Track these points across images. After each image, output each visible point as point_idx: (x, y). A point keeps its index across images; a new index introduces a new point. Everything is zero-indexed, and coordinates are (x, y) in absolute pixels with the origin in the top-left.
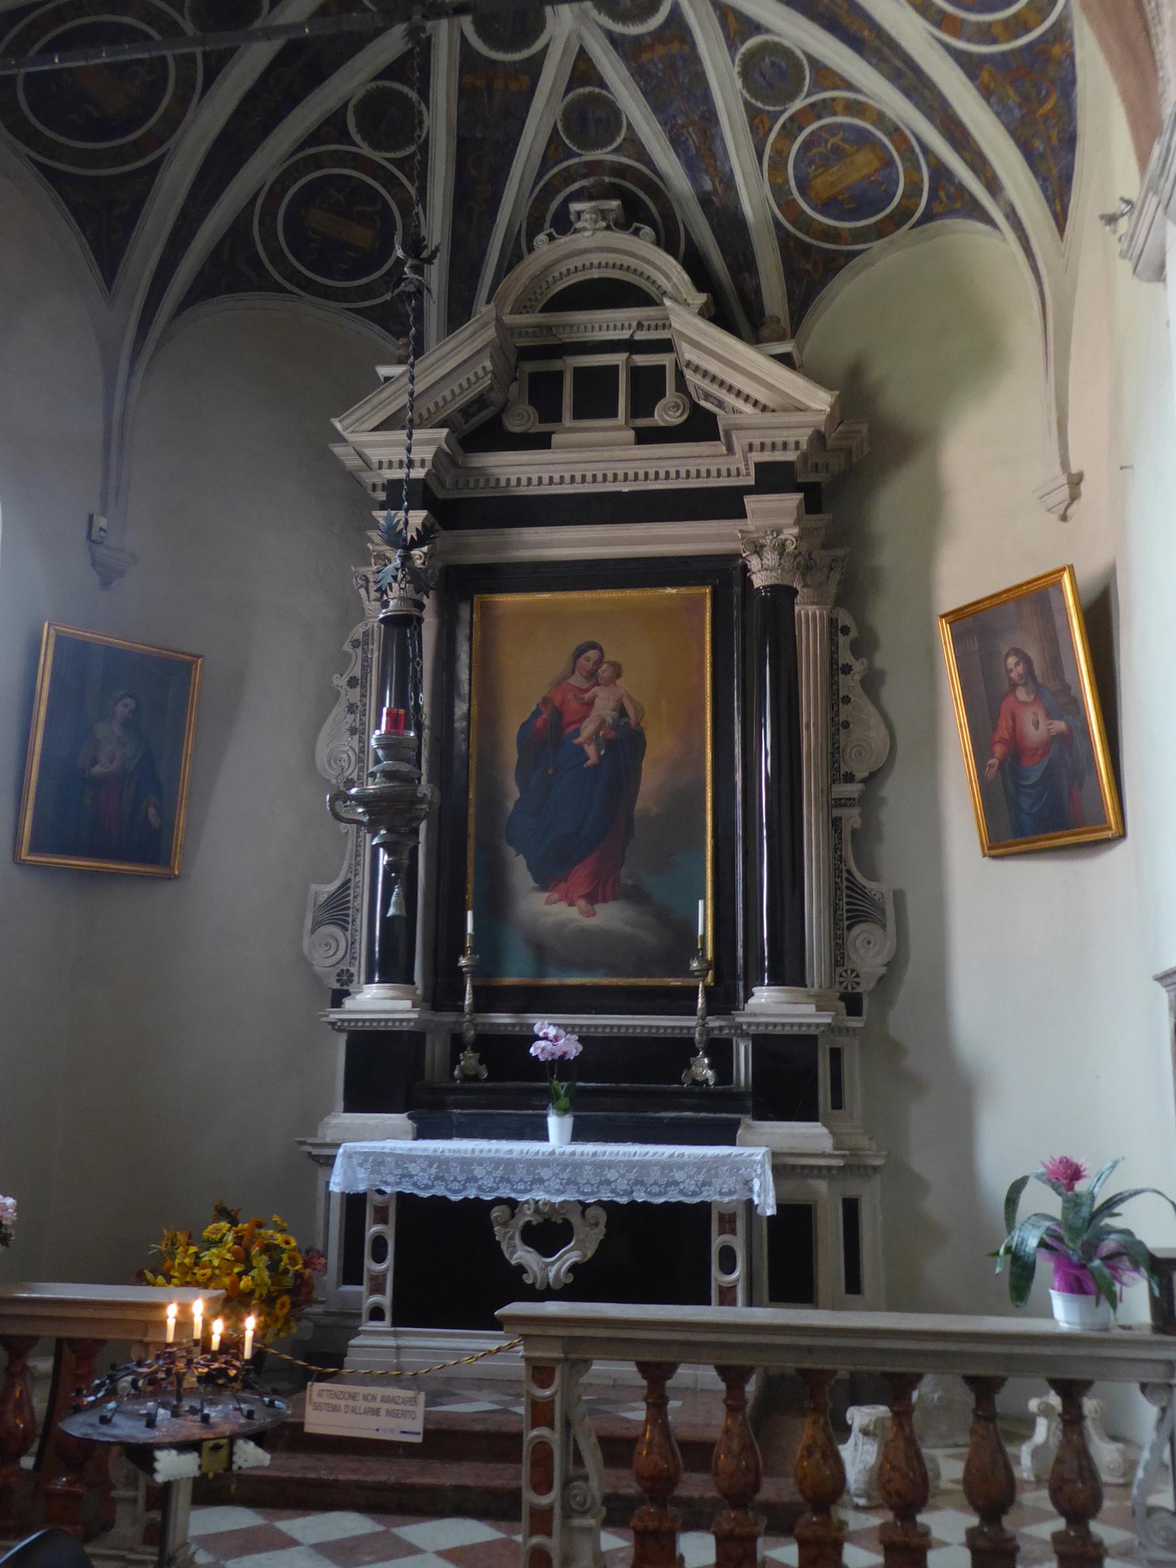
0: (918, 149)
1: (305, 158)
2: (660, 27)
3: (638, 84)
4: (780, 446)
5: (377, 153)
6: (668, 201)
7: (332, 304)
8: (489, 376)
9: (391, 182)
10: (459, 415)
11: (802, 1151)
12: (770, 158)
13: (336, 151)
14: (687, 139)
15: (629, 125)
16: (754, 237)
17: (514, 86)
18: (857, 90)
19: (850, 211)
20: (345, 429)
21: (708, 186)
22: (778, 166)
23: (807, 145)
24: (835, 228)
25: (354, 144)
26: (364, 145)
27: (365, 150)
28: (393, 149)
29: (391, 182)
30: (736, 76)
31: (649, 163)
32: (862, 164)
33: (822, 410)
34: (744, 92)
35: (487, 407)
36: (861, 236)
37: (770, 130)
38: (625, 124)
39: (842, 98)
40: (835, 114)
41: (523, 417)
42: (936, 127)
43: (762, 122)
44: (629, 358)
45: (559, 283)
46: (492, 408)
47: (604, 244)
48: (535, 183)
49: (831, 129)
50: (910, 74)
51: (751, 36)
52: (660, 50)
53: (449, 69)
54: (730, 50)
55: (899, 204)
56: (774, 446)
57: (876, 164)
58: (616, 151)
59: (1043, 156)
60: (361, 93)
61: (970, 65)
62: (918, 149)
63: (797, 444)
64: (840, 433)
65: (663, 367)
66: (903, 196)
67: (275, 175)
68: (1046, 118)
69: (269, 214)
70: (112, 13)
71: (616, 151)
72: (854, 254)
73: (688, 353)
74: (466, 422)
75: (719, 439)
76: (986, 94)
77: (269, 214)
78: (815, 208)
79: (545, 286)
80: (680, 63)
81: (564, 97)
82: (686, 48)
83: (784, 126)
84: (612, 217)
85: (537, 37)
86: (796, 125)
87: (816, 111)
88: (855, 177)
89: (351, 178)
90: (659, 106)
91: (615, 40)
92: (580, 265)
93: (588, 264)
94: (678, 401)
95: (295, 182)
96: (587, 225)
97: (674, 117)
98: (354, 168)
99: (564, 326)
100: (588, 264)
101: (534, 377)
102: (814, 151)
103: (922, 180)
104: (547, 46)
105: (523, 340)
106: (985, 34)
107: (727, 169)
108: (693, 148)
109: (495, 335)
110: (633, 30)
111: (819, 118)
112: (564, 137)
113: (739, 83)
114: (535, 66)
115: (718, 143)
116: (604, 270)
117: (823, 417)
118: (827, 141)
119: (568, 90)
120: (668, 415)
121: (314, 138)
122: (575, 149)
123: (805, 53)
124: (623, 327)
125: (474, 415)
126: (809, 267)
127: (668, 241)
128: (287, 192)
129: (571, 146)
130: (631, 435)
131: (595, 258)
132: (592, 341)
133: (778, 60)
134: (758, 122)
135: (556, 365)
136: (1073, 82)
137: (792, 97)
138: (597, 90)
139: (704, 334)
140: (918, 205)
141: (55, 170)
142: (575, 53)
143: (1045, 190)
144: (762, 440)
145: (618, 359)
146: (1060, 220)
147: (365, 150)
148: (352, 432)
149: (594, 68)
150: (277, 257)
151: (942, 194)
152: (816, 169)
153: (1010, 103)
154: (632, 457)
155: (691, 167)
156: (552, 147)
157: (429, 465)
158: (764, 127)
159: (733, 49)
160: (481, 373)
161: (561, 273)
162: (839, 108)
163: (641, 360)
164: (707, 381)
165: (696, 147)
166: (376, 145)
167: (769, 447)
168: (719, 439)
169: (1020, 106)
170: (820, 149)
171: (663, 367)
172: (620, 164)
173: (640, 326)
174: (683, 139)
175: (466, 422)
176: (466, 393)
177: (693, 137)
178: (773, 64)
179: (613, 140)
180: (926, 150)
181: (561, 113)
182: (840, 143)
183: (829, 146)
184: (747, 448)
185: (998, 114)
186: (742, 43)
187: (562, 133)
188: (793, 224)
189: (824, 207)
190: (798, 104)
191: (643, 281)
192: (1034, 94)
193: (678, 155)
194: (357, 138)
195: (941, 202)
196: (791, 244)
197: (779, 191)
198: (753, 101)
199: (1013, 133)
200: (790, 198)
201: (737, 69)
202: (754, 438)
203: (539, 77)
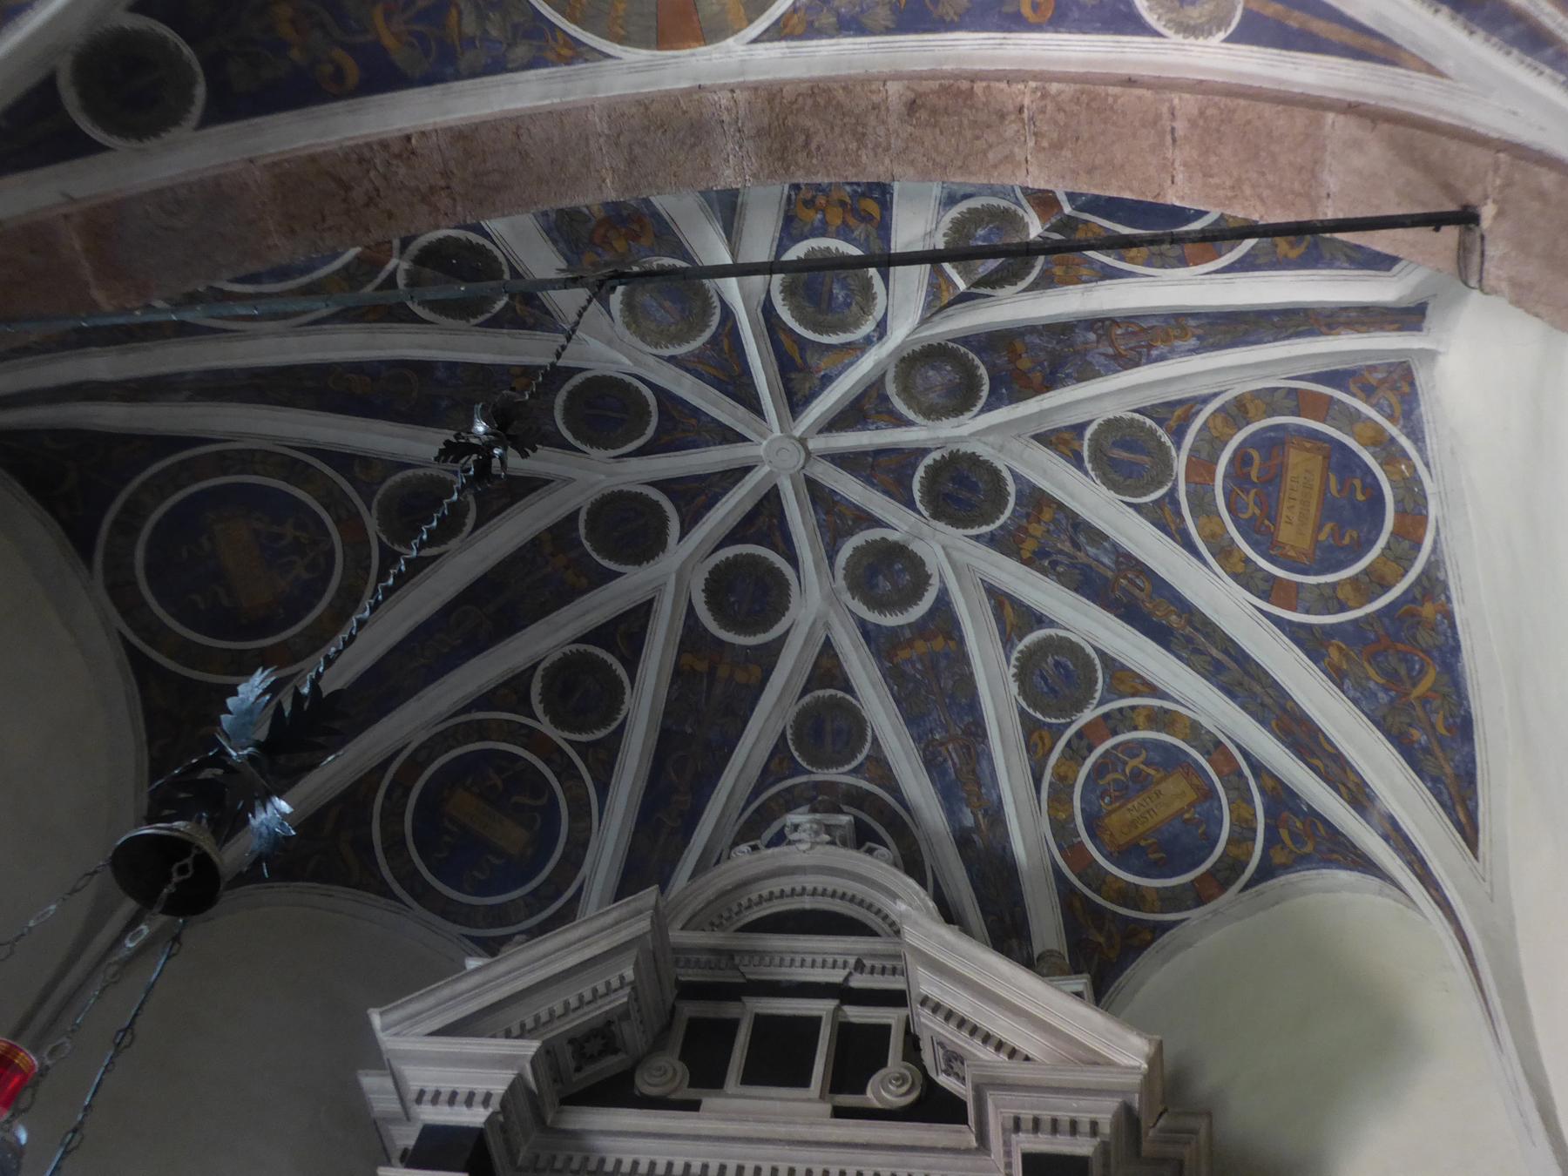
0: (1247, 771)
1: (468, 723)
2: (922, 617)
3: (891, 690)
4: (1065, 1126)
5: (559, 732)
6: (915, 841)
7: (449, 926)
8: (627, 990)
9: (566, 771)
10: (568, 1050)
11: (723, 1134)
12: (1051, 784)
13: (508, 722)
14: (945, 760)
15: (875, 740)
16: (1027, 888)
17: (740, 677)
18: (1164, 696)
19: (1156, 863)
20: (385, 1028)
21: (969, 821)
22: (1060, 795)
23: (1099, 770)
24: (1137, 886)
25: (534, 717)
26: (546, 720)
27: (546, 726)
28: (579, 729)
29: (566, 771)
30: (1011, 679)
31: (895, 789)
32: (1173, 795)
33: (1133, 1068)
34: (1020, 700)
35: (615, 1051)
36: (1173, 900)
37: (1051, 749)
38: (869, 738)
39: (1144, 707)
40: (1135, 728)
41: (665, 1073)
42: (1271, 731)
43: (1041, 738)
44: (838, 1008)
45: (755, 909)
46: (621, 1056)
47: (827, 862)
48: (748, 803)
49: (1131, 748)
50: (1232, 665)
51: (1031, 630)
52: (921, 646)
53: (667, 639)
54: (1004, 647)
55: (1225, 853)
56: (1055, 1126)
57: (1192, 796)
58: (854, 771)
59: (1427, 750)
60: (557, 655)
61: (1310, 642)
62: (1247, 771)
63: (1094, 1125)
64: (1162, 1130)
65: (887, 1028)
66: (1229, 842)
67: (423, 737)
68: (1424, 700)
69: (402, 784)
70: (286, 480)
71: (854, 771)
72: (1166, 927)
73: (926, 984)
74: (578, 1069)
75: (965, 1121)
76: (1337, 677)
77: (402, 784)
78: (1108, 857)
79: (735, 909)
80: (943, 663)
81: (799, 698)
82: (952, 644)
83: (1069, 744)
84: (838, 833)
85: (777, 620)
86: (1084, 743)
87: (1111, 723)
88: (1163, 814)
89: (518, 758)
90: (913, 717)
91: (868, 633)
92: (788, 889)
93: (798, 889)
94: (907, 1073)
95: (446, 752)
96: (804, 836)
97: (931, 730)
98: (525, 747)
99: (752, 953)
100: (798, 889)
101: (694, 1024)
102: (1110, 777)
103: (1255, 815)
104: (787, 632)
105: (690, 971)
106: (1330, 600)
107: (995, 796)
108: (952, 771)
109: (649, 928)
110: (890, 620)
111: (1115, 733)
112: (792, 748)
113: (1014, 688)
114: (768, 656)
115: (984, 764)
116: (820, 970)
117: (1136, 1079)
118: (1125, 763)
119: (805, 691)
120: (888, 1091)
121: (485, 700)
122: (804, 764)
123: (1096, 649)
124: (834, 965)
125: (592, 1059)
126: (1101, 940)
127: (913, 864)
128: (433, 760)
129: (799, 760)
130: (828, 1108)
131: (810, 881)
132: (790, 981)
133: (1063, 660)
134: (1036, 738)
135: (730, 1010)
136: (1456, 649)
137: (1079, 706)
138: (840, 694)
139: (953, 950)
140: (1250, 854)
141: (146, 657)
142: (820, 644)
143: (1437, 795)
144: (1036, 1112)
145: (822, 1008)
146: (1469, 832)
147: (546, 726)
148: (396, 1034)
149: (840, 666)
150: (394, 845)
151: (1284, 834)
152: (1111, 803)
153: (1372, 685)
154: (824, 1138)
155: (949, 796)
156: (776, 760)
157: (495, 1105)
158: (1044, 744)
159: (1009, 646)
160: (615, 983)
161: (760, 896)
162: (1141, 720)
163: (857, 1014)
164: (952, 1026)
165: (955, 772)
166: (558, 722)
167: (1046, 1126)
168: (965, 1121)
169: (1386, 690)
170: (1117, 776)
171: (887, 1028)
172: (858, 789)
173: (859, 966)
174: (940, 759)
175: (578, 1069)
176: (586, 1009)
177: (952, 757)
178: (1057, 664)
179: (854, 757)
180: (1258, 768)
181: (792, 718)
182: (1142, 766)
183: (1127, 771)
184: (1010, 1124)
185: (1355, 701)
186: (1020, 640)
187: (790, 743)
188: (1080, 878)
189: (1121, 856)
190: (1088, 715)
191: (872, 916)
192: (1403, 672)
193: (933, 783)
194: (538, 709)
195: (1284, 847)
196: (1077, 904)
197: (1062, 829)
198: (1031, 711)
199: (1379, 723)
200: (1076, 840)
201: (1013, 670)
202: (1023, 1107)
203: (773, 669)
